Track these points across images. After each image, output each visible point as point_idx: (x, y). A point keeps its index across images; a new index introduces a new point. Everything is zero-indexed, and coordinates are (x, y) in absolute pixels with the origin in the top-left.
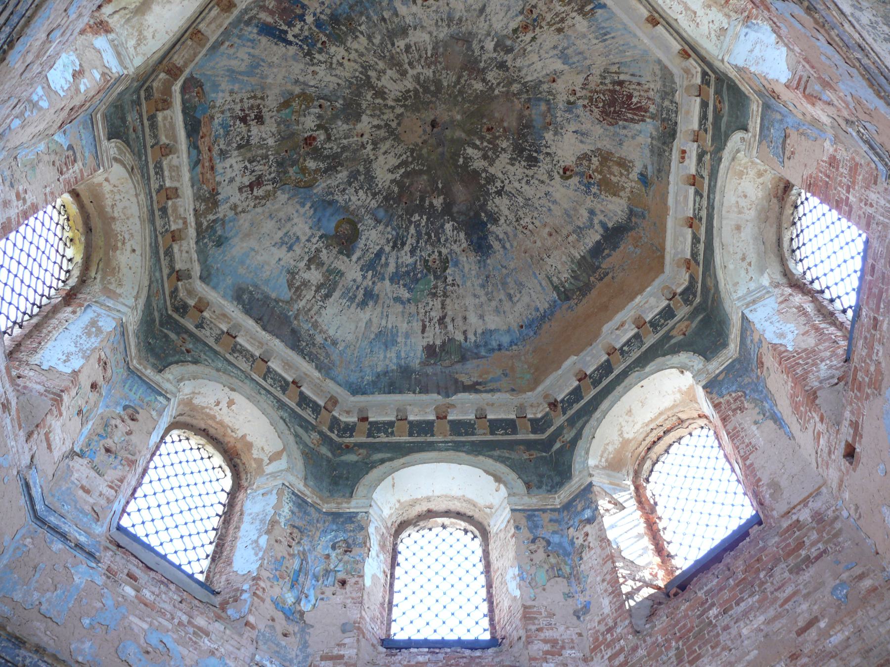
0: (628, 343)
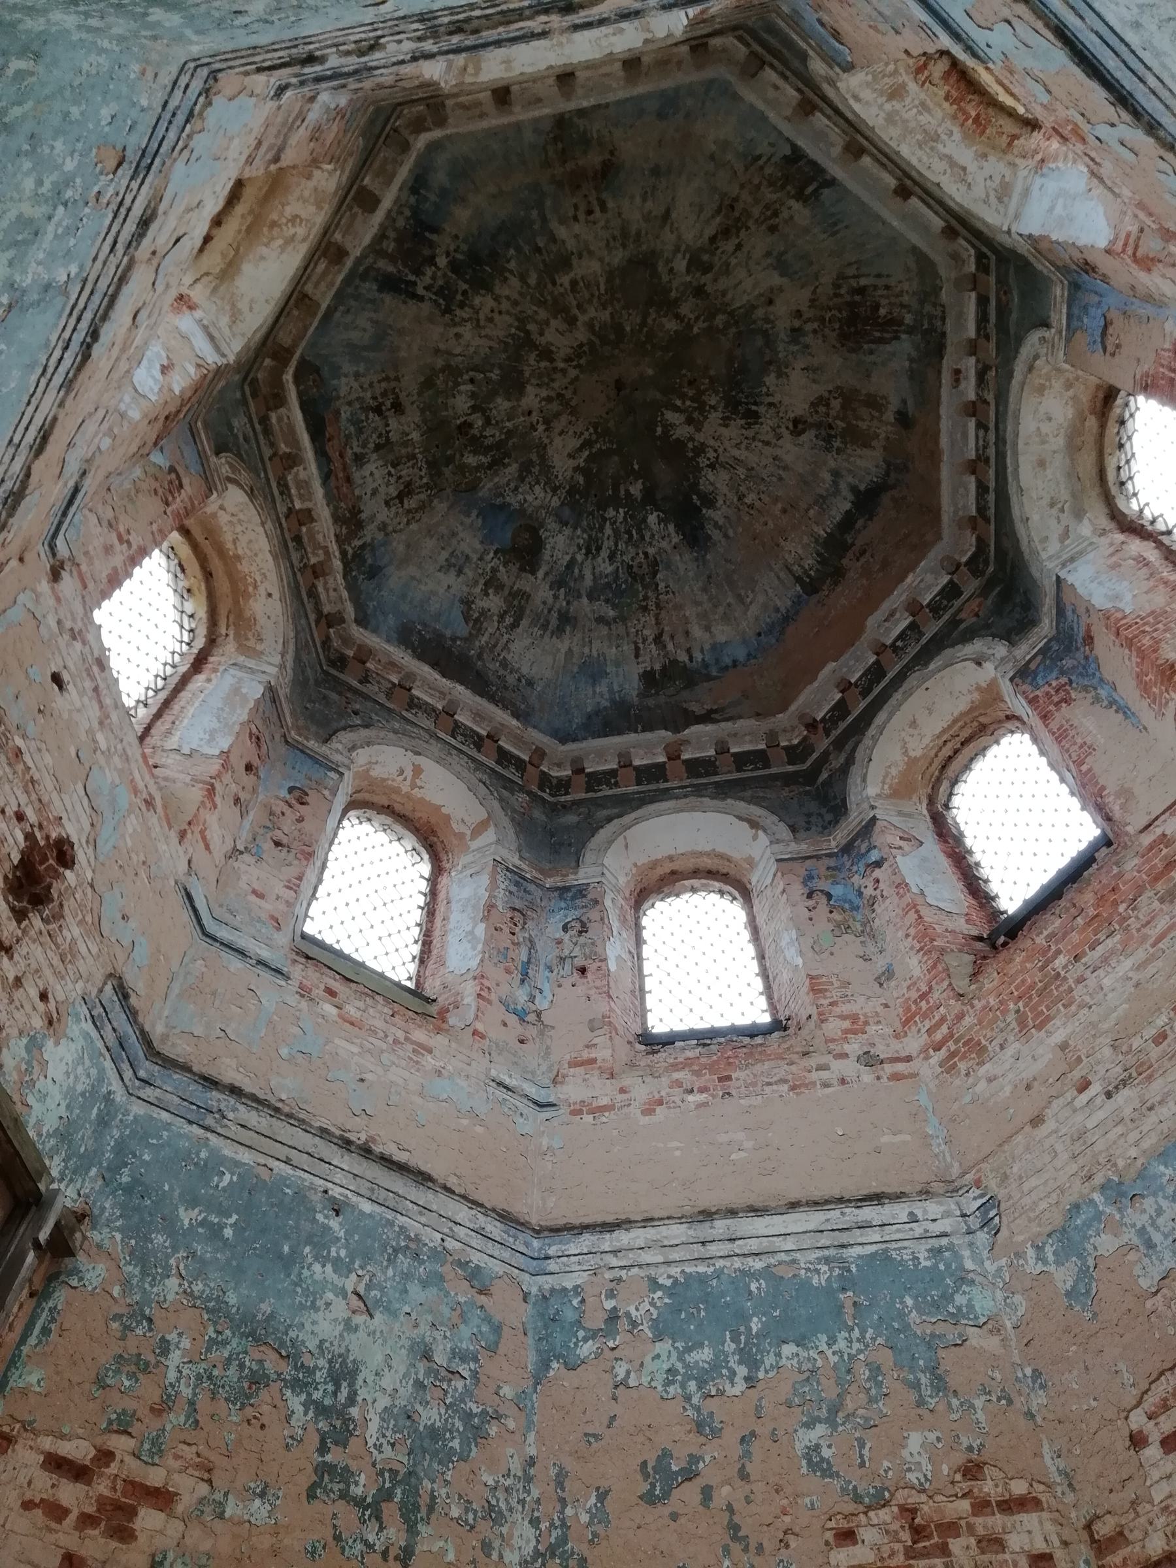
0: (901, 636)
